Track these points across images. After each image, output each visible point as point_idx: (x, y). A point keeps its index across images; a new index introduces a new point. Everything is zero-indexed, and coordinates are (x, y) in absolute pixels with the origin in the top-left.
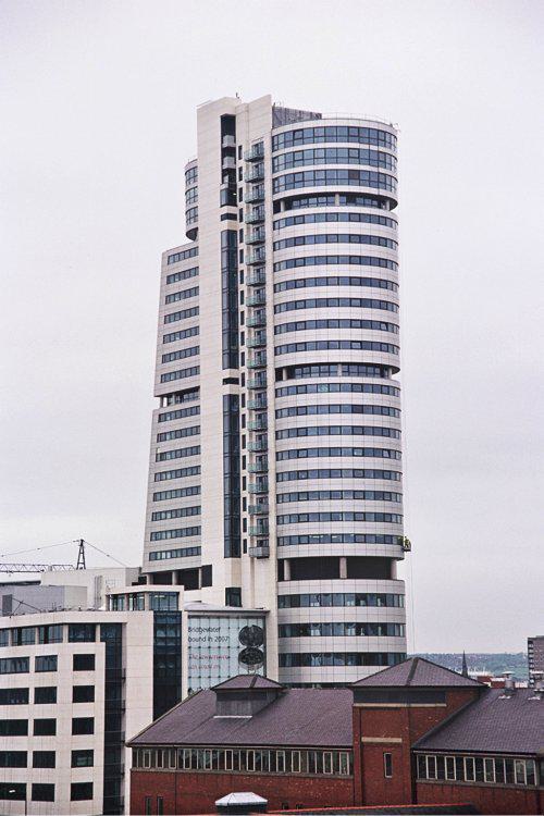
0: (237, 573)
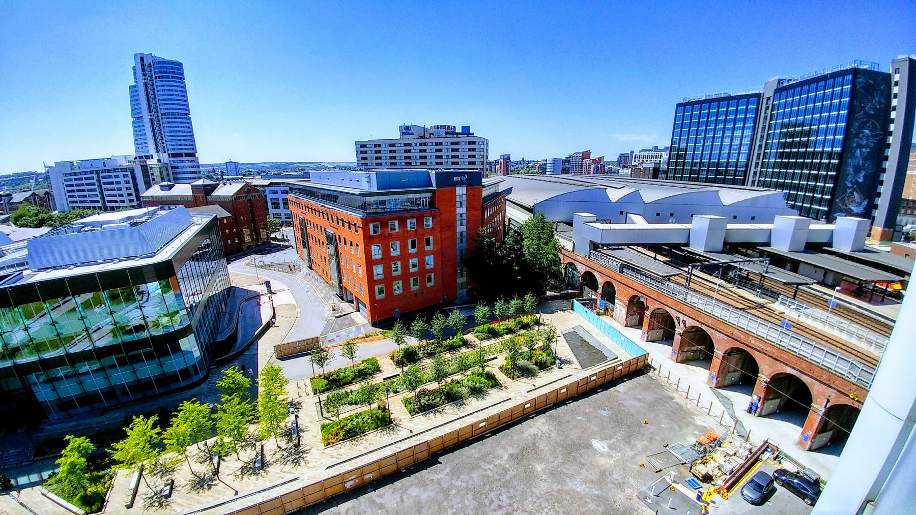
0: (159, 156)
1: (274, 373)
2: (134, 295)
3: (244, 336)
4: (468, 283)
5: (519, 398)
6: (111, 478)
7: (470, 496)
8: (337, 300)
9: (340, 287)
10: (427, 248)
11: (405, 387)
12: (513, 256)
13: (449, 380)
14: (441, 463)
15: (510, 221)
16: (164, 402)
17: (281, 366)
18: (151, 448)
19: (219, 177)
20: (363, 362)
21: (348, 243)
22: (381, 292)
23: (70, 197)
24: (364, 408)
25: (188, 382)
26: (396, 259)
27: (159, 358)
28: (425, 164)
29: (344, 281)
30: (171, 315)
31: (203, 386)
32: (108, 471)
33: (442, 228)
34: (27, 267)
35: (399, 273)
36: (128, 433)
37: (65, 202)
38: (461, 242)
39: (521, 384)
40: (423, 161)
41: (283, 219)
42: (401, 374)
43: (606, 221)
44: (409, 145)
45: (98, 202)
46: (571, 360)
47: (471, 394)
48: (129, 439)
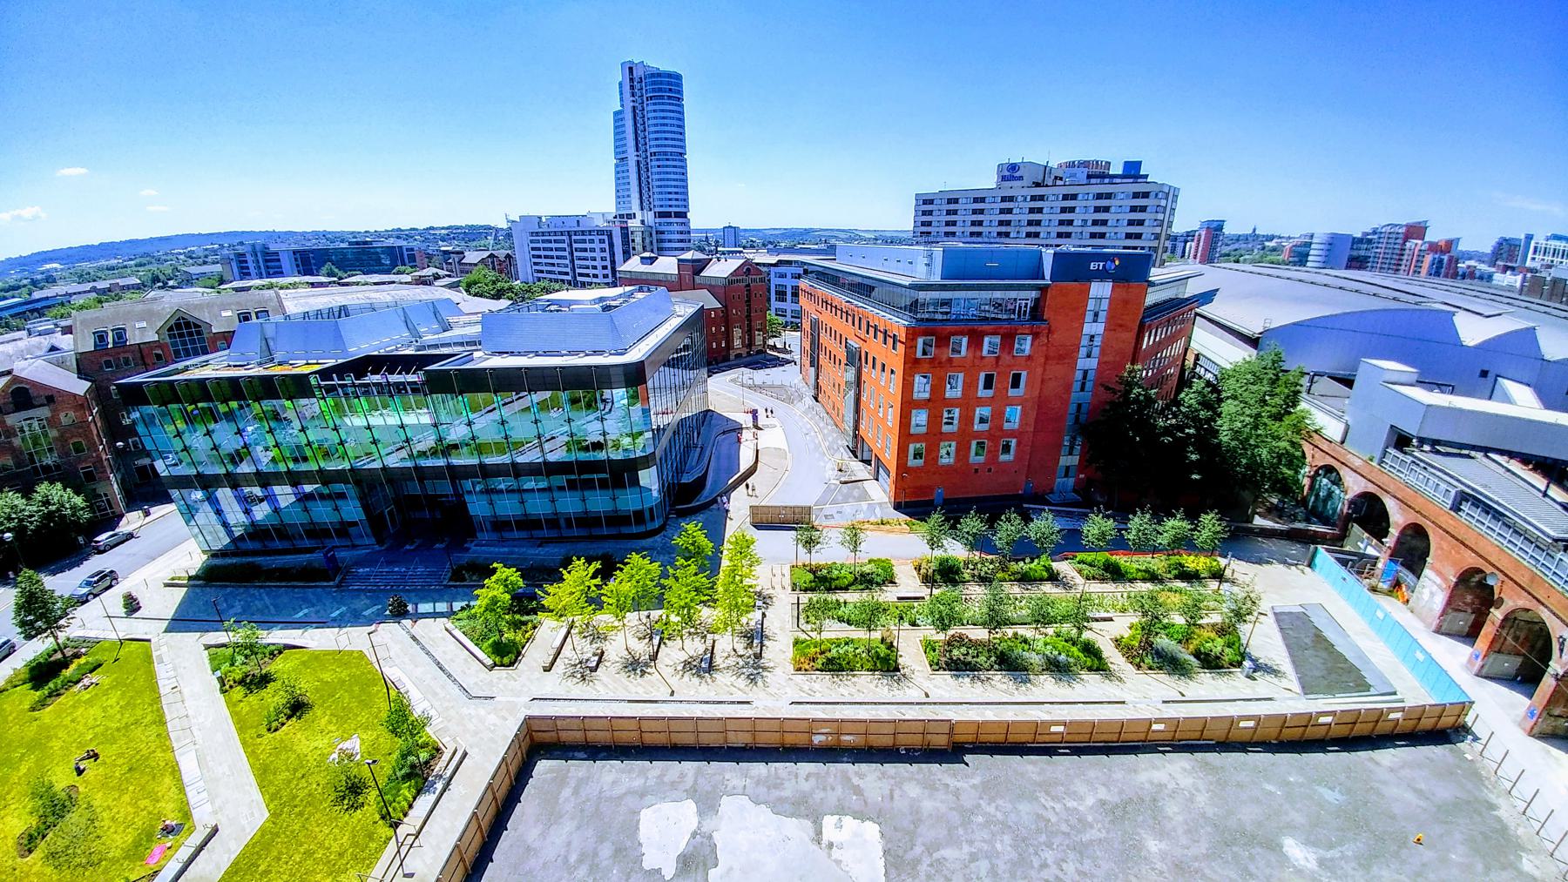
0: (643, 215)
1: (745, 544)
2: (596, 402)
3: (715, 482)
4: (1081, 467)
5: (1143, 706)
6: (535, 628)
7: (1007, 839)
8: (847, 455)
9: (855, 436)
10: (1012, 392)
11: (929, 621)
12: (1192, 431)
13: (1010, 632)
14: (967, 765)
15: (1197, 357)
16: (609, 547)
17: (755, 538)
18: (586, 602)
19: (713, 248)
20: (870, 562)
21: (879, 366)
22: (917, 455)
23: (535, 264)
24: (859, 634)
25: (642, 529)
26: (952, 403)
27: (613, 489)
28: (1037, 235)
29: (862, 427)
30: (634, 436)
31: (657, 538)
32: (532, 617)
33: (1047, 358)
34: (479, 347)
35: (954, 428)
36: (565, 577)
37: (529, 271)
38: (1082, 389)
39: (1155, 683)
40: (1032, 229)
41: (789, 319)
42: (927, 598)
43: (1441, 387)
44: (1011, 199)
45: (567, 274)
46: (1282, 669)
47: (1047, 670)
48: (565, 583)
